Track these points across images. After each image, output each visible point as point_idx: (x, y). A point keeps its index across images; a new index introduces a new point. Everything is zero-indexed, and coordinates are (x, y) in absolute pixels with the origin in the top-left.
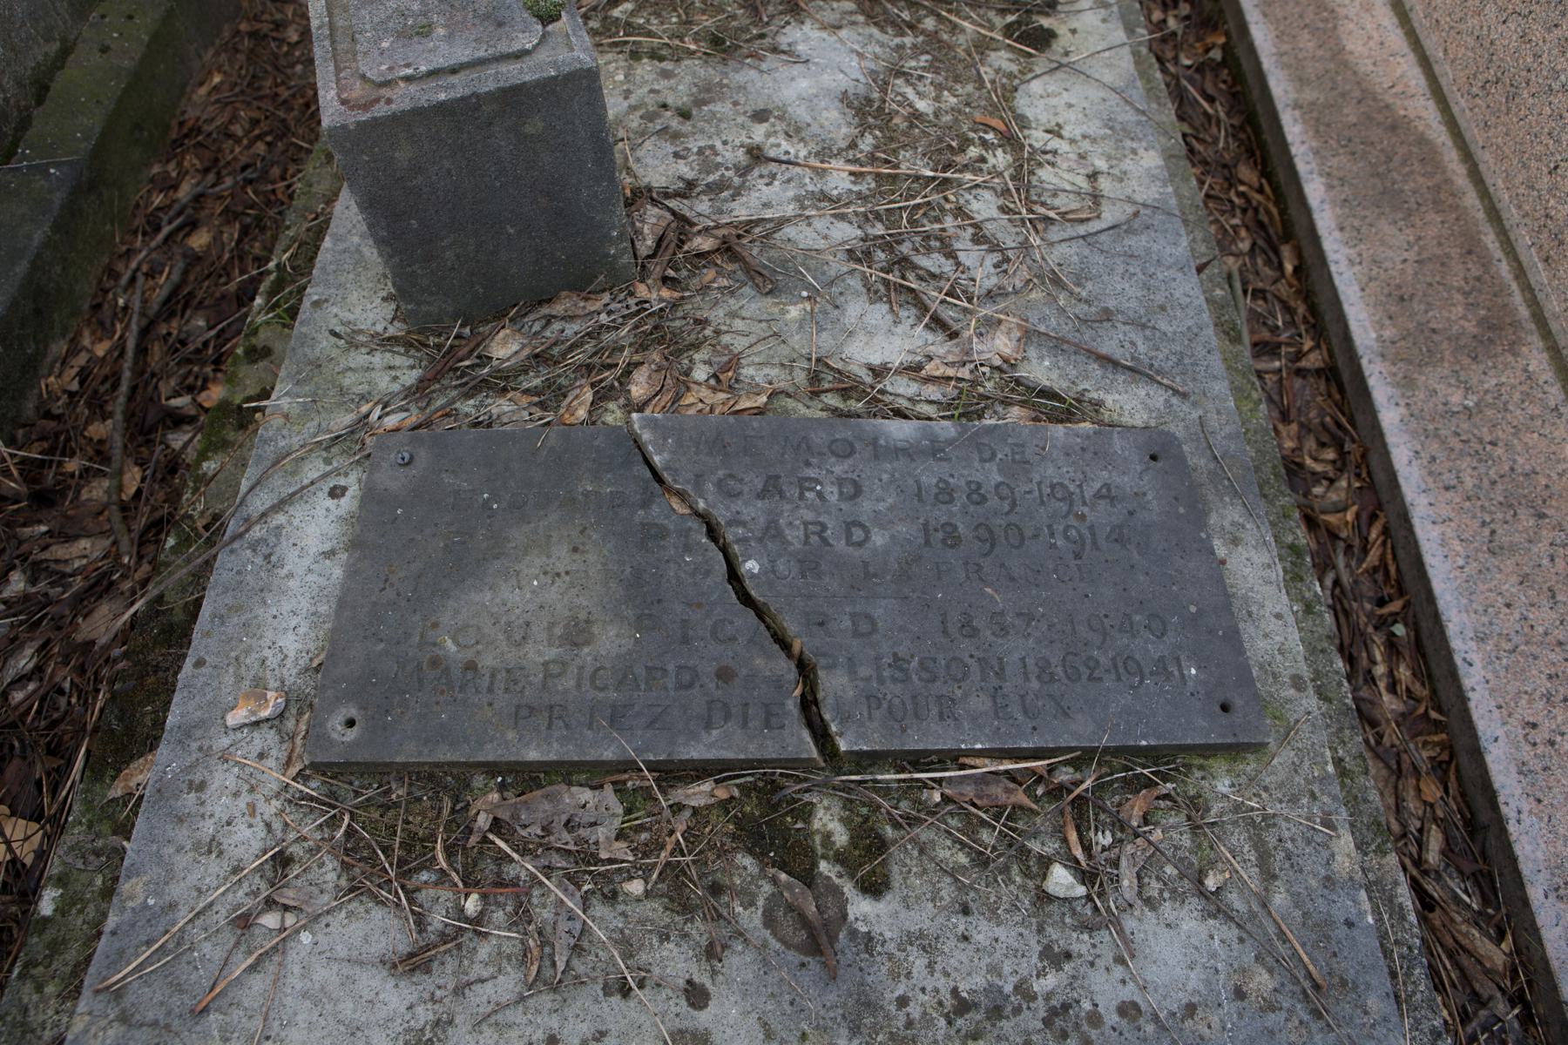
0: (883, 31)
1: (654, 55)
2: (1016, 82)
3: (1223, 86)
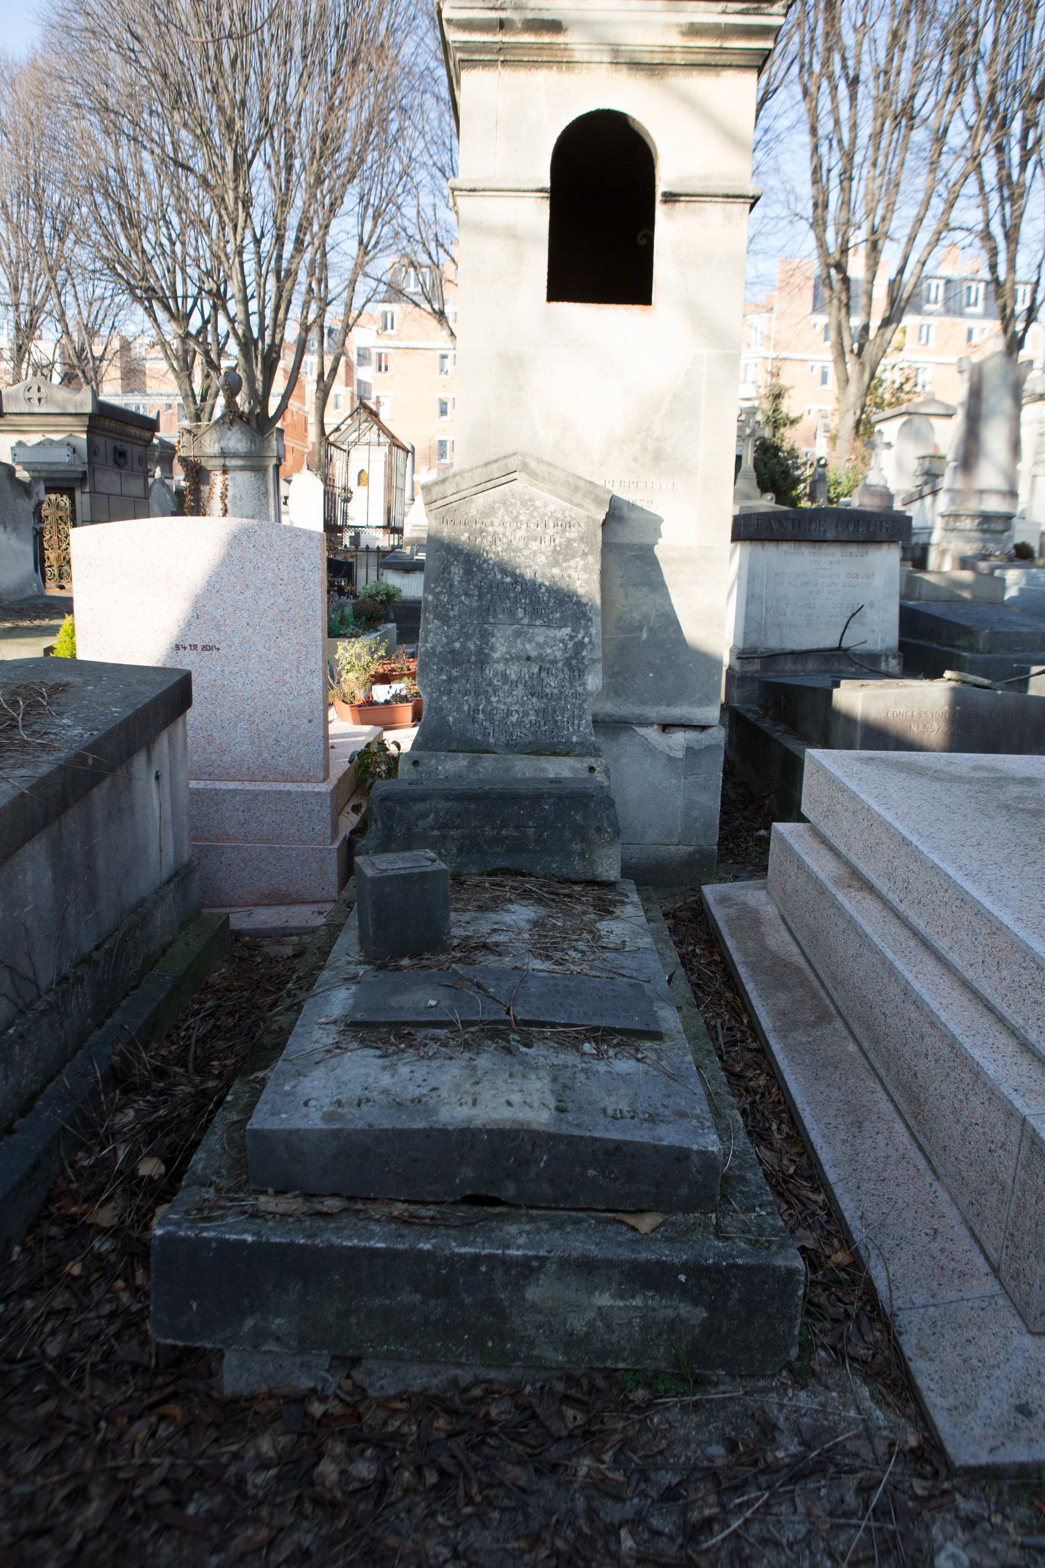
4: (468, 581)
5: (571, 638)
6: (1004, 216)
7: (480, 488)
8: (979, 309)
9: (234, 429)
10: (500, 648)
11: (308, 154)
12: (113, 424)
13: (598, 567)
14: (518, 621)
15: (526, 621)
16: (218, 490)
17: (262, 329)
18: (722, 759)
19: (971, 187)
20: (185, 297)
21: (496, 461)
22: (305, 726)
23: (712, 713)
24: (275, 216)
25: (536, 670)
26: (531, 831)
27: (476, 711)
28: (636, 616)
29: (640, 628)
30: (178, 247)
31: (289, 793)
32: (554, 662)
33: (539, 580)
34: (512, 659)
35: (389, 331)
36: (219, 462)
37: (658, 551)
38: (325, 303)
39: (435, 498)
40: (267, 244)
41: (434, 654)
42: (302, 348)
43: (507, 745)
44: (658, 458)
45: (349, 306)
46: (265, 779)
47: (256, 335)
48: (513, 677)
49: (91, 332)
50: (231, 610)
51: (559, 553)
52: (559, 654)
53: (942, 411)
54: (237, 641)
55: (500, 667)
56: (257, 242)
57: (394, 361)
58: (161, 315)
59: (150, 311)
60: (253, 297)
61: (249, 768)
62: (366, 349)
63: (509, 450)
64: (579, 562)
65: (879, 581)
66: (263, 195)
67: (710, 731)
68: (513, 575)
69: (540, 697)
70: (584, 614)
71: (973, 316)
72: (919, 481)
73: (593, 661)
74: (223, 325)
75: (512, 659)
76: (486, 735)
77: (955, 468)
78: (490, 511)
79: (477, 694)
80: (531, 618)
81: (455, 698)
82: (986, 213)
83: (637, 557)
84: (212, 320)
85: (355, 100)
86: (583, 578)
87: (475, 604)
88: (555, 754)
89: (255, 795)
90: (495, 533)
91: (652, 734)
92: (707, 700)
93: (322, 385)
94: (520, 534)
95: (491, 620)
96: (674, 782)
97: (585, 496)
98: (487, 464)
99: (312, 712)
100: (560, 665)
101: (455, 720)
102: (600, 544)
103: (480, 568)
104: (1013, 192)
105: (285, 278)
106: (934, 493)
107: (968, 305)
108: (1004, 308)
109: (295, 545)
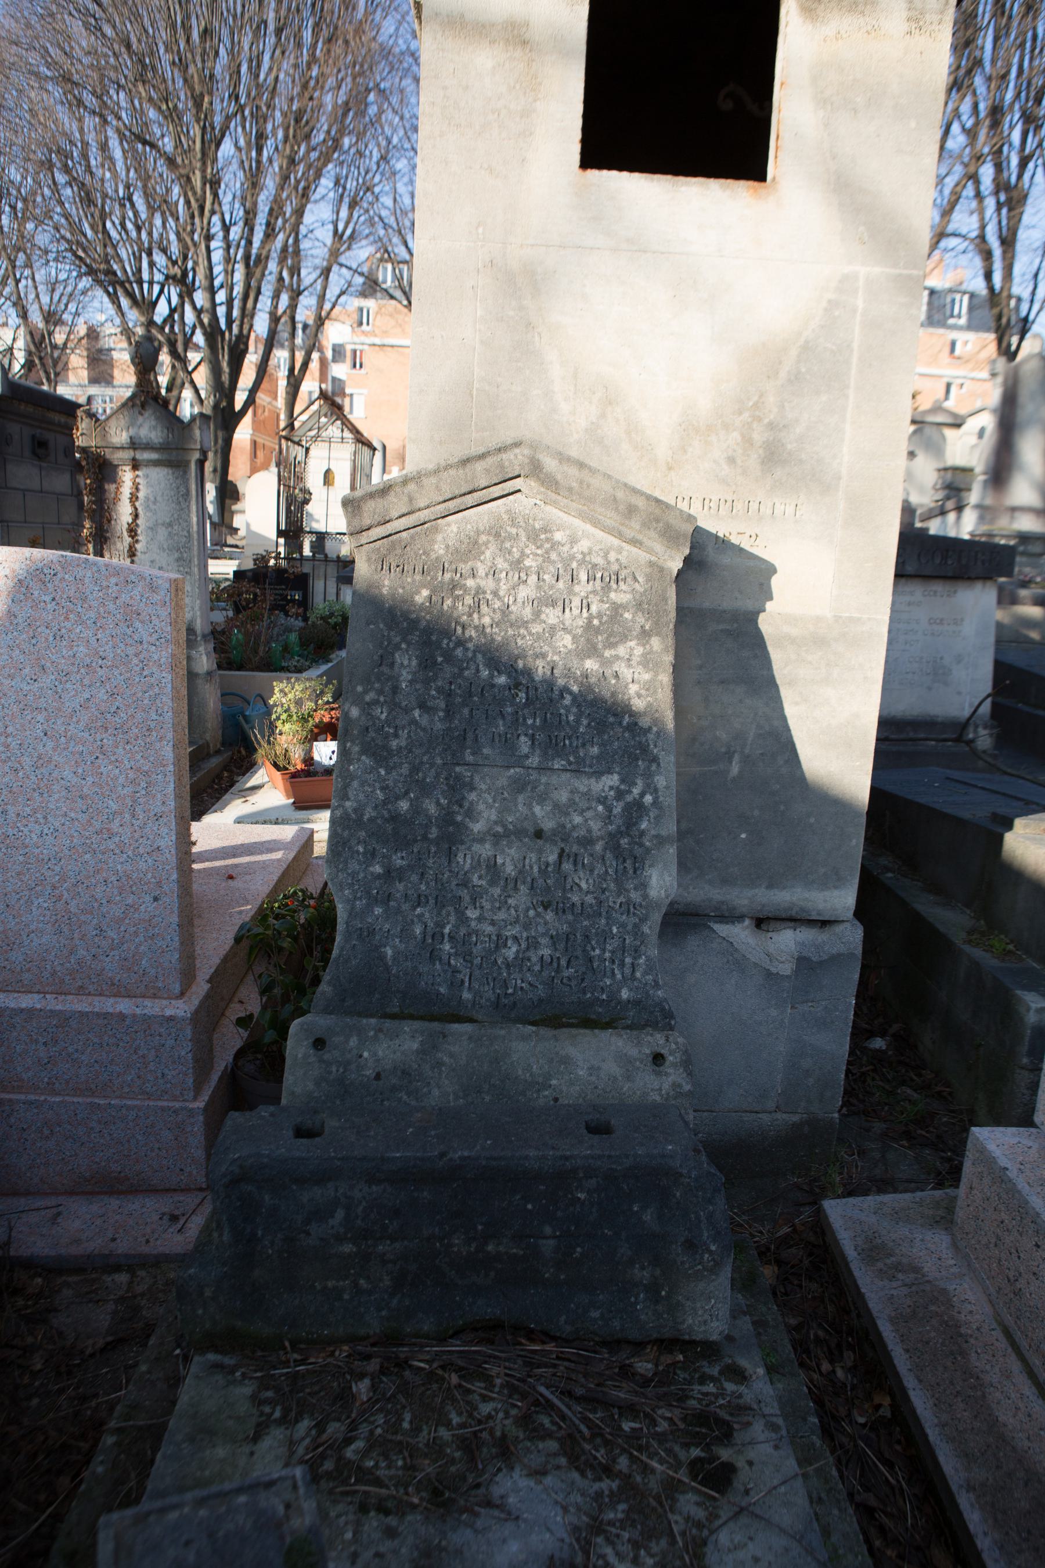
0: (583, 1474)
1: (383, 1510)
2: (705, 1532)
3: (898, 1448)
4: (427, 682)
5: (620, 795)
6: (1000, 222)
7: (452, 505)
8: (963, 321)
9: (147, 414)
10: (485, 813)
11: (280, 134)
12: (30, 409)
13: (669, 658)
14: (519, 761)
15: (534, 761)
16: (126, 490)
17: (230, 321)
18: (857, 976)
19: (969, 191)
20: (151, 283)
21: (482, 457)
22: (147, 906)
23: (844, 899)
24: (244, 199)
25: (552, 858)
26: (548, 1246)
27: (438, 936)
28: (722, 735)
29: (729, 756)
30: (144, 235)
31: (122, 1016)
32: (587, 841)
33: (561, 682)
34: (507, 834)
35: (364, 327)
36: (128, 455)
37: (765, 624)
38: (296, 294)
39: (367, 522)
40: (235, 233)
41: (359, 823)
42: (270, 344)
43: (497, 1005)
44: (776, 457)
45: (322, 298)
46: (81, 991)
47: (223, 326)
48: (510, 870)
49: (52, 318)
50: (15, 708)
51: (597, 631)
52: (595, 826)
53: (949, 420)
54: (27, 761)
55: (485, 850)
56: (226, 229)
57: (370, 358)
58: (125, 302)
59: (114, 299)
60: (222, 286)
61: (54, 973)
62: (341, 346)
63: (508, 436)
64: (633, 648)
65: (969, 628)
66: (233, 182)
67: (839, 929)
68: (511, 670)
69: (563, 909)
70: (644, 749)
71: (955, 327)
72: (940, 495)
73: (661, 841)
74: (190, 316)
75: (507, 834)
76: (456, 985)
77: (985, 482)
78: (471, 548)
79: (440, 904)
80: (544, 754)
81: (398, 911)
82: (982, 219)
83: (728, 633)
84: (179, 310)
85: (331, 82)
86: (641, 676)
87: (439, 726)
88: (589, 1023)
89: (64, 1019)
90: (479, 591)
91: (741, 934)
92: (833, 880)
93: (292, 380)
94: (523, 592)
95: (470, 758)
96: (774, 1012)
97: (645, 525)
98: (465, 462)
99: (159, 884)
100: (599, 847)
101: (397, 953)
102: (673, 615)
103: (449, 657)
104: (1013, 199)
105: (254, 265)
106: (960, 509)
107: (952, 316)
108: (999, 317)
109: (124, 598)
